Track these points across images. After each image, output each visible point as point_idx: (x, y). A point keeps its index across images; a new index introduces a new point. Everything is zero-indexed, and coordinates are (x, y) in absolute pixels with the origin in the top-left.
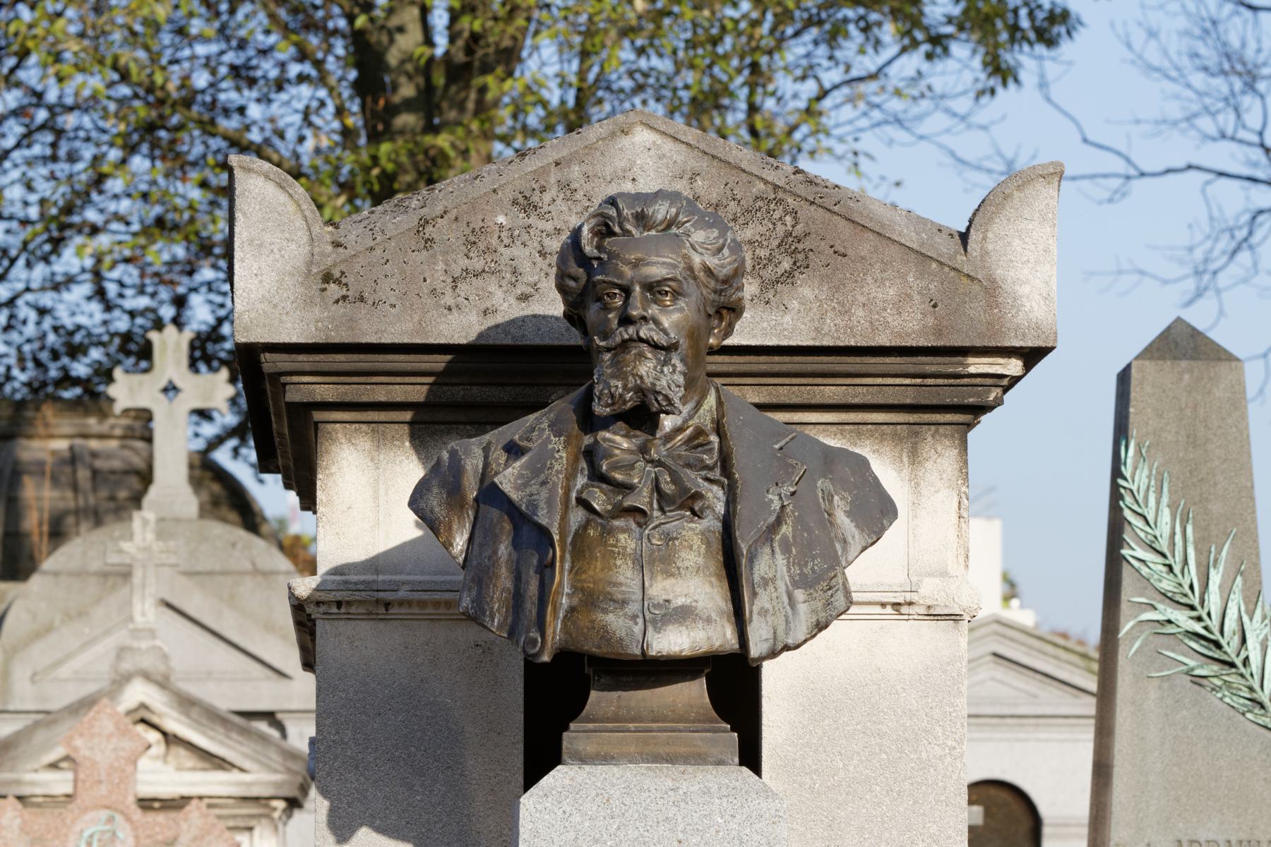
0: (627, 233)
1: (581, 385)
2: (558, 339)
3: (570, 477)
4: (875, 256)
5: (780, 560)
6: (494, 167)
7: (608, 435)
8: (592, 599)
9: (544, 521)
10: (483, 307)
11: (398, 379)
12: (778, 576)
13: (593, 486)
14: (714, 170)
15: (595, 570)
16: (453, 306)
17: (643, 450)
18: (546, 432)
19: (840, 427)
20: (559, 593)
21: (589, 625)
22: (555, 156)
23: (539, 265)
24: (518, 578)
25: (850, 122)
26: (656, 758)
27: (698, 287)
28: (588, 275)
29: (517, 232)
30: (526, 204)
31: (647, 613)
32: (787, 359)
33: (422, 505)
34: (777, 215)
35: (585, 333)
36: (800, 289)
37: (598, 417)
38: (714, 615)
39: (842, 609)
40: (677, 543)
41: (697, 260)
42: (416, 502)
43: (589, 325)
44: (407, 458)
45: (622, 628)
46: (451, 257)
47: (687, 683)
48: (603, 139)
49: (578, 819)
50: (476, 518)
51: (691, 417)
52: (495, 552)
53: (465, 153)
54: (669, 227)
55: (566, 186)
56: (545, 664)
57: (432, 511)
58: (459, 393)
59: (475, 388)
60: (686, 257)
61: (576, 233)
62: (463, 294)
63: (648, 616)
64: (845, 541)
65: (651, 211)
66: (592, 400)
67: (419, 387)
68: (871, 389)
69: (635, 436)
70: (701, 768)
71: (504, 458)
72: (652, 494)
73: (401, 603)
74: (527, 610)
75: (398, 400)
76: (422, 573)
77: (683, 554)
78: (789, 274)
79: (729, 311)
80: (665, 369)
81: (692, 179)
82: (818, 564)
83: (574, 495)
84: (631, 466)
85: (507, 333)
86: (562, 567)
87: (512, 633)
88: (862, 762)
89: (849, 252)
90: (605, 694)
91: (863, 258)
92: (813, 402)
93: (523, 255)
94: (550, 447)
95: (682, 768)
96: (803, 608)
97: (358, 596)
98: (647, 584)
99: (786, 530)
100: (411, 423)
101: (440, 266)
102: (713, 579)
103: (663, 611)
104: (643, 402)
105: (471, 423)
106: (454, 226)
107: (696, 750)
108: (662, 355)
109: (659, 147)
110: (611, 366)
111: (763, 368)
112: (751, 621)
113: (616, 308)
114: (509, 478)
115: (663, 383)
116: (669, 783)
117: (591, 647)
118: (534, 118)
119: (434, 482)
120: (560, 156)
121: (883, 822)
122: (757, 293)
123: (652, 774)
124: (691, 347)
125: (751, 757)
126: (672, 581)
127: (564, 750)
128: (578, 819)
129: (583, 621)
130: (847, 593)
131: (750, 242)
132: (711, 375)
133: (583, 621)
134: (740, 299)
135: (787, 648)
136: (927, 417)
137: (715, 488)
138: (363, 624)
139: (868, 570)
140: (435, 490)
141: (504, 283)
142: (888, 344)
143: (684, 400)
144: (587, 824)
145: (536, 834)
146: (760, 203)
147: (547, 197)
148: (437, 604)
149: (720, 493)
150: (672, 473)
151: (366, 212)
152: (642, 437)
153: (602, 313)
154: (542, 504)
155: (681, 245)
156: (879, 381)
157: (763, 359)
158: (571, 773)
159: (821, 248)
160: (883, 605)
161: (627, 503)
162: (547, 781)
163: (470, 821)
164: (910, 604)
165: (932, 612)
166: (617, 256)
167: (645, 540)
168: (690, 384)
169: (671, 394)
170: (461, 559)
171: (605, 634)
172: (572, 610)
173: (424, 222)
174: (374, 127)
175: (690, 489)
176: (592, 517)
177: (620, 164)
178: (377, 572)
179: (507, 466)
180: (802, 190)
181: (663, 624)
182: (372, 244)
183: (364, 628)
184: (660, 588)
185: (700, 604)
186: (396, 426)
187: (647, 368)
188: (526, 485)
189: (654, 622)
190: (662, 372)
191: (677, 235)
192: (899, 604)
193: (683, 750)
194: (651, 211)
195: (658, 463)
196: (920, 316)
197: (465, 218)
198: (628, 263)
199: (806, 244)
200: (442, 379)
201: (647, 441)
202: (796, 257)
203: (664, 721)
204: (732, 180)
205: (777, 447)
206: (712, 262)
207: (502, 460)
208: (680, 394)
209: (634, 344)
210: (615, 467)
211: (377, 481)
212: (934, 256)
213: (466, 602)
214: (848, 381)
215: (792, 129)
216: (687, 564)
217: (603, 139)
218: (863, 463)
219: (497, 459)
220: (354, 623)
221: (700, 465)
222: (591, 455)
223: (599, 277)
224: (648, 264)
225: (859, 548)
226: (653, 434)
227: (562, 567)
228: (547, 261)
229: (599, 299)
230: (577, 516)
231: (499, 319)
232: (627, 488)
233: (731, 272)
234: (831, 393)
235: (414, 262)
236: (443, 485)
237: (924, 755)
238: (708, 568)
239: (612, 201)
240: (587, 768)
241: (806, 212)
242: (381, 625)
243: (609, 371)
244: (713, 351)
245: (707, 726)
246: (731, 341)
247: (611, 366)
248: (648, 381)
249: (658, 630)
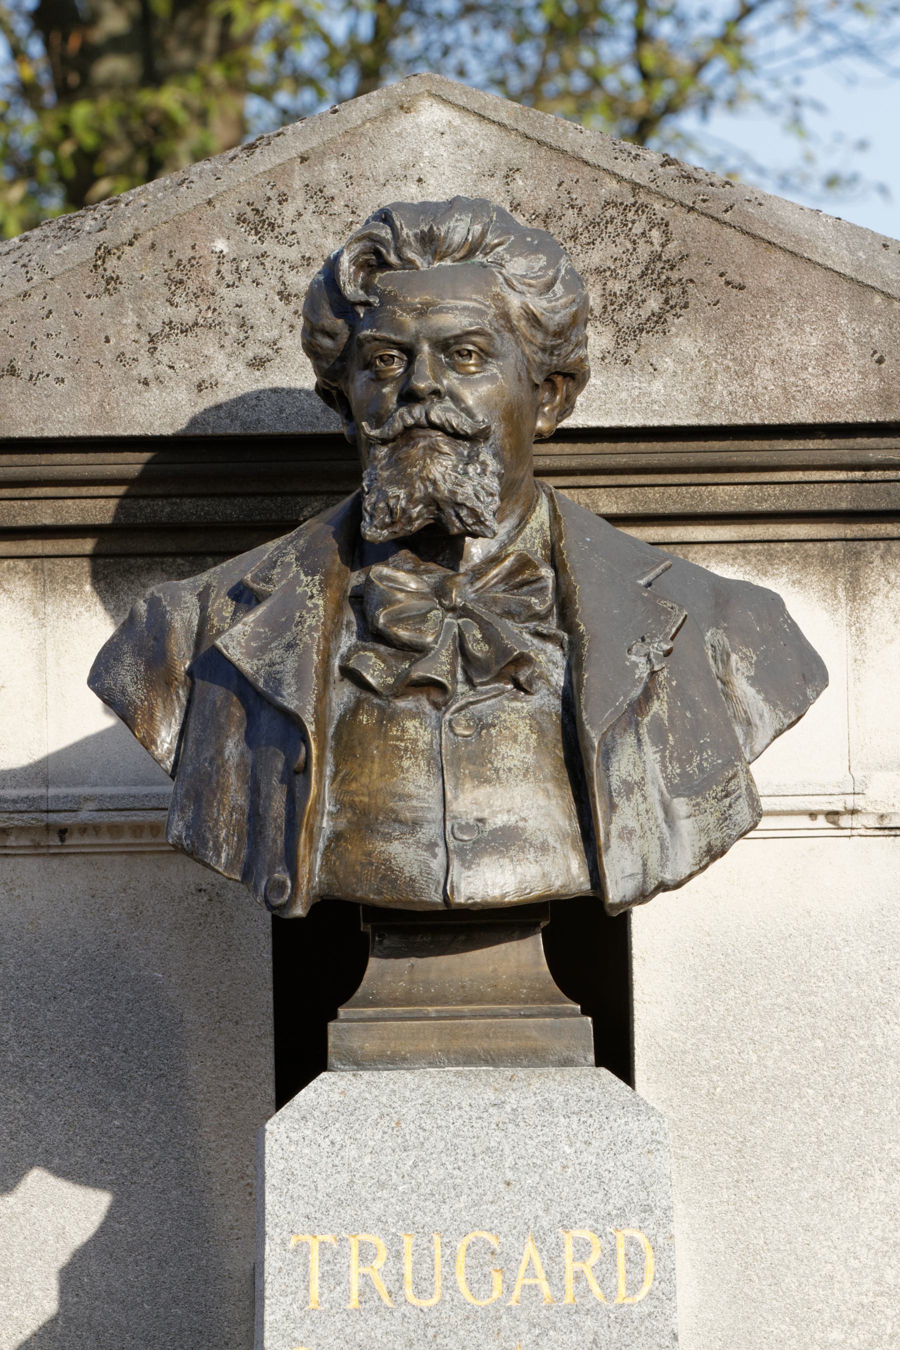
0: (408, 264)
1: (348, 493)
2: (311, 424)
3: (331, 635)
5: (651, 754)
8: (366, 820)
9: (291, 704)
10: (196, 379)
11: (71, 491)
13: (365, 649)
14: (541, 164)
15: (371, 777)
16: (151, 377)
17: (440, 592)
18: (291, 568)
19: (742, 547)
20: (317, 811)
21: (363, 859)
23: (278, 313)
24: (255, 790)
25: (790, 51)
26: (470, 1058)
27: (518, 343)
28: (350, 327)
30: (258, 222)
33: (109, 682)
34: (637, 229)
35: (349, 416)
37: (371, 544)
38: (551, 841)
39: (746, 826)
40: (493, 731)
41: (515, 302)
42: (100, 679)
43: (353, 405)
44: (88, 609)
45: (415, 864)
48: (372, 120)
49: (354, 1153)
50: (189, 701)
51: (512, 540)
52: (220, 751)
53: (202, 117)
54: (471, 253)
55: (317, 193)
56: (298, 920)
57: (123, 692)
58: (163, 510)
59: (187, 501)
60: (498, 298)
61: (332, 266)
62: (165, 360)
64: (749, 723)
65: (443, 229)
66: (361, 518)
67: (102, 502)
68: (786, 488)
69: (428, 572)
70: (538, 1071)
71: (231, 609)
72: (454, 658)
73: (83, 829)
74: (267, 841)
75: (72, 521)
76: (115, 783)
77: (503, 749)
78: (659, 318)
80: (471, 469)
81: (508, 178)
82: (709, 758)
83: (336, 663)
84: (423, 618)
86: (321, 773)
87: (247, 875)
88: (786, 1052)
89: (749, 282)
91: (769, 291)
92: (700, 510)
94: (299, 590)
95: (509, 1072)
96: (686, 826)
97: (18, 820)
98: (449, 795)
99: (659, 707)
100: (93, 557)
101: (131, 319)
102: (550, 786)
104: (438, 520)
105: (183, 554)
106: (150, 258)
107: (531, 1043)
108: (465, 448)
109: (457, 130)
111: (623, 460)
112: (608, 847)
113: (394, 378)
114: (237, 640)
117: (367, 892)
118: (308, 55)
121: (820, 1143)
122: (611, 346)
124: (509, 435)
125: (615, 1052)
126: (487, 789)
127: (330, 1049)
128: (354, 1153)
129: (354, 853)
131: (598, 271)
132: (539, 473)
134: (583, 360)
135: (663, 887)
136: (873, 529)
137: (550, 647)
138: (28, 861)
142: (810, 420)
143: (500, 515)
144: (367, 1160)
145: (290, 1177)
146: (612, 212)
147: (289, 210)
148: (137, 829)
150: (484, 626)
151: (16, 240)
152: (438, 572)
154: (289, 678)
155: (490, 280)
156: (799, 476)
157: (622, 446)
158: (342, 1084)
159: (706, 278)
160: (813, 815)
162: (305, 1096)
164: (853, 812)
165: (886, 823)
166: (394, 300)
167: (445, 729)
168: (509, 489)
169: (480, 507)
170: (169, 764)
171: (388, 873)
172: (337, 836)
173: (104, 253)
174: (65, 80)
175: (511, 650)
177: (399, 157)
178: (47, 783)
179: (234, 620)
180: (674, 190)
182: (26, 287)
183: (29, 869)
184: (469, 802)
185: (531, 824)
186: (70, 562)
187: (442, 468)
188: (263, 649)
189: (461, 853)
190: (466, 473)
192: (837, 813)
193: (510, 1044)
194: (443, 229)
195: (462, 612)
196: (857, 377)
198: (412, 309)
200: (137, 488)
201: (446, 578)
202: (667, 291)
203: (481, 1001)
204: (569, 177)
205: (642, 582)
206: (538, 305)
207: (228, 612)
208: (494, 507)
209: (422, 433)
210: (398, 619)
211: (43, 645)
212: (878, 285)
213: (178, 828)
215: (700, 65)
216: (509, 763)
217: (372, 120)
218: (774, 603)
219: (220, 610)
220: (12, 861)
221: (525, 613)
222: (360, 601)
223: (368, 332)
225: (771, 733)
226: (454, 567)
227: (321, 773)
228: (292, 307)
229: (368, 365)
230: (342, 695)
231: (221, 396)
232: (415, 651)
233: (567, 319)
235: (91, 312)
236: (139, 652)
237: (879, 1041)
238: (541, 768)
239: (384, 216)
240: (366, 1075)
241: (683, 222)
242: (55, 863)
243: (385, 474)
244: (541, 439)
245: (545, 1007)
246: (574, 421)
248: (445, 488)
249: (467, 865)
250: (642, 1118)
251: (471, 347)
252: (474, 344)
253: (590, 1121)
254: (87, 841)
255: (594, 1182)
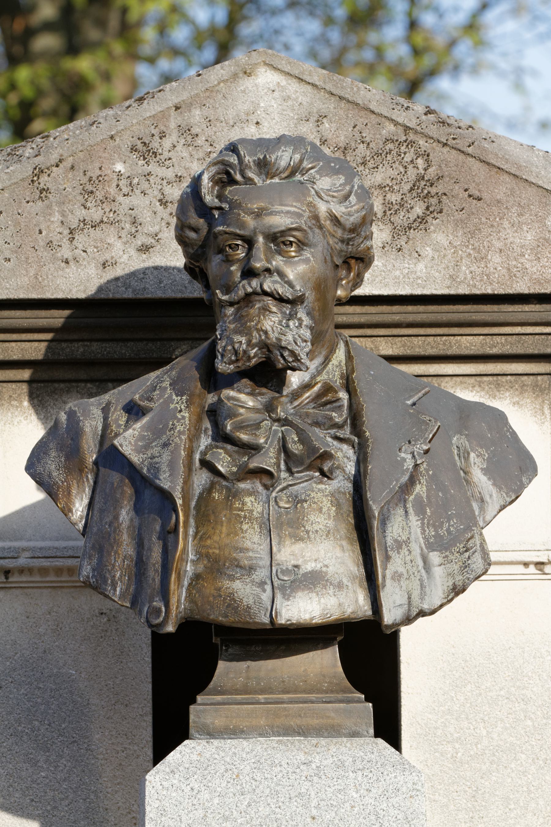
0: (249, 181)
2: (181, 291)
3: (194, 438)
4: (511, 199)
5: (414, 521)
6: (110, 112)
7: (232, 393)
8: (217, 566)
9: (166, 485)
10: (101, 260)
11: (15, 336)
12: (413, 537)
13: (217, 447)
14: (341, 112)
15: (220, 536)
16: (70, 258)
17: (270, 408)
18: (166, 392)
19: (478, 379)
20: (183, 559)
22: (175, 100)
23: (159, 215)
24: (140, 545)
26: (288, 731)
27: (324, 236)
28: (208, 225)
29: (135, 181)
30: (145, 151)
31: (275, 579)
32: (421, 308)
33: (40, 469)
34: (408, 158)
35: (207, 286)
36: (434, 236)
37: (222, 374)
38: (345, 581)
39: (480, 572)
40: (305, 505)
41: (322, 208)
42: (34, 467)
43: (210, 278)
44: (26, 418)
46: (66, 208)
47: (319, 652)
49: (207, 796)
50: (95, 483)
51: (319, 372)
52: (116, 517)
53: (107, 77)
54: (292, 174)
56: (169, 634)
57: (50, 476)
59: (95, 344)
61: (196, 182)
62: (80, 246)
63: (276, 583)
64: (482, 500)
65: (273, 157)
66: (215, 357)
67: (36, 344)
68: (509, 338)
69: (261, 394)
70: (335, 740)
72: (279, 454)
73: (21, 571)
74: (149, 580)
75: (15, 357)
76: (43, 539)
77: (312, 517)
78: (422, 220)
79: (357, 260)
80: (291, 323)
82: (455, 525)
83: (197, 457)
84: (257, 426)
85: (127, 286)
87: (135, 603)
89: (485, 195)
90: (234, 664)
91: (499, 202)
92: (449, 353)
93: (143, 204)
94: (172, 406)
95: (314, 741)
96: (438, 572)
98: (275, 549)
99: (420, 489)
101: (57, 217)
102: (344, 543)
103: (292, 578)
104: (268, 358)
106: (70, 175)
108: (287, 309)
109: (283, 89)
110: (235, 321)
112: (384, 586)
113: (239, 260)
115: (288, 339)
116: (302, 757)
117: (217, 615)
118: (180, 35)
119: (51, 445)
120: (179, 99)
121: (529, 792)
123: (283, 747)
124: (318, 300)
125: (388, 728)
126: (300, 545)
128: (207, 796)
129: (209, 589)
130: (485, 554)
131: (381, 187)
132: (338, 326)
133: (209, 589)
134: (369, 249)
135: (422, 613)
137: (345, 447)
139: (507, 530)
140: (53, 454)
141: (123, 234)
142: (526, 292)
143: (311, 355)
144: (216, 801)
145: (163, 812)
146: (390, 146)
147: (167, 143)
148: (59, 571)
149: (350, 452)
150: (300, 432)
152: (268, 394)
153: (224, 265)
154: (164, 467)
155: (306, 193)
157: (396, 308)
158: (199, 748)
159: (455, 192)
161: (253, 464)
162: (173, 756)
163: (97, 797)
166: (239, 206)
167: (272, 503)
168: (317, 337)
169: (297, 350)
170: (81, 526)
171: (232, 602)
172: (197, 577)
173: (38, 172)
176: (217, 479)
177: (243, 107)
179: (127, 426)
180: (433, 131)
181: (293, 591)
184: (289, 553)
186: (14, 386)
187: (272, 323)
188: (147, 447)
189: (283, 589)
190: (288, 326)
191: (301, 183)
192: (543, 563)
193: (315, 722)
195: (285, 422)
197: (82, 167)
198: (251, 212)
199: (439, 188)
200: (61, 334)
201: (273, 398)
202: (429, 200)
203: (295, 692)
204: (361, 122)
205: (409, 402)
206: (339, 210)
207: (123, 421)
208: (307, 350)
209: (257, 298)
210: (240, 427)
213: (87, 570)
214: (486, 330)
216: (316, 527)
218: (500, 418)
219: (117, 420)
222: (214, 414)
223: (221, 228)
224: (271, 214)
225: (497, 507)
226: (279, 391)
228: (169, 210)
229: (221, 251)
230: (201, 479)
231: (119, 272)
232: (252, 449)
233: (359, 220)
234: (468, 343)
236: (61, 448)
238: (338, 530)
239: (233, 148)
240: (216, 742)
241: (439, 154)
243: (232, 326)
244: (340, 303)
245: (340, 696)
246: (361, 291)
247: (235, 321)
249: (287, 597)
250: (407, 773)
251: (292, 239)
252: (294, 236)
253: (371, 775)
254: (24, 579)
255: (373, 817)
